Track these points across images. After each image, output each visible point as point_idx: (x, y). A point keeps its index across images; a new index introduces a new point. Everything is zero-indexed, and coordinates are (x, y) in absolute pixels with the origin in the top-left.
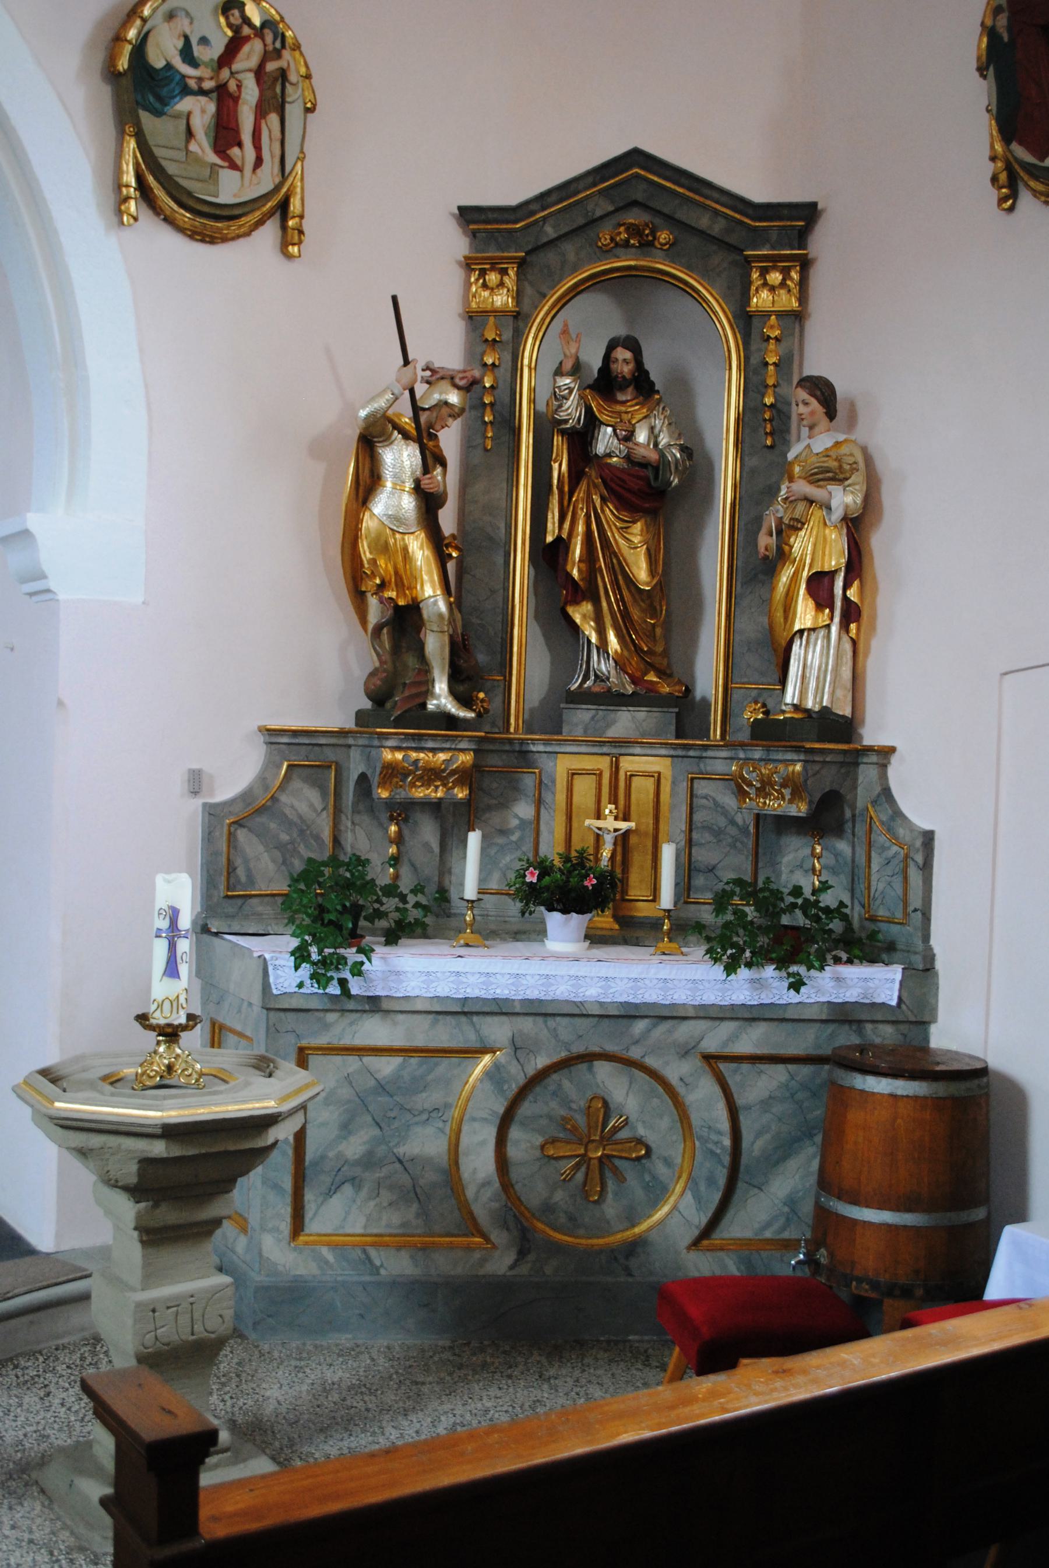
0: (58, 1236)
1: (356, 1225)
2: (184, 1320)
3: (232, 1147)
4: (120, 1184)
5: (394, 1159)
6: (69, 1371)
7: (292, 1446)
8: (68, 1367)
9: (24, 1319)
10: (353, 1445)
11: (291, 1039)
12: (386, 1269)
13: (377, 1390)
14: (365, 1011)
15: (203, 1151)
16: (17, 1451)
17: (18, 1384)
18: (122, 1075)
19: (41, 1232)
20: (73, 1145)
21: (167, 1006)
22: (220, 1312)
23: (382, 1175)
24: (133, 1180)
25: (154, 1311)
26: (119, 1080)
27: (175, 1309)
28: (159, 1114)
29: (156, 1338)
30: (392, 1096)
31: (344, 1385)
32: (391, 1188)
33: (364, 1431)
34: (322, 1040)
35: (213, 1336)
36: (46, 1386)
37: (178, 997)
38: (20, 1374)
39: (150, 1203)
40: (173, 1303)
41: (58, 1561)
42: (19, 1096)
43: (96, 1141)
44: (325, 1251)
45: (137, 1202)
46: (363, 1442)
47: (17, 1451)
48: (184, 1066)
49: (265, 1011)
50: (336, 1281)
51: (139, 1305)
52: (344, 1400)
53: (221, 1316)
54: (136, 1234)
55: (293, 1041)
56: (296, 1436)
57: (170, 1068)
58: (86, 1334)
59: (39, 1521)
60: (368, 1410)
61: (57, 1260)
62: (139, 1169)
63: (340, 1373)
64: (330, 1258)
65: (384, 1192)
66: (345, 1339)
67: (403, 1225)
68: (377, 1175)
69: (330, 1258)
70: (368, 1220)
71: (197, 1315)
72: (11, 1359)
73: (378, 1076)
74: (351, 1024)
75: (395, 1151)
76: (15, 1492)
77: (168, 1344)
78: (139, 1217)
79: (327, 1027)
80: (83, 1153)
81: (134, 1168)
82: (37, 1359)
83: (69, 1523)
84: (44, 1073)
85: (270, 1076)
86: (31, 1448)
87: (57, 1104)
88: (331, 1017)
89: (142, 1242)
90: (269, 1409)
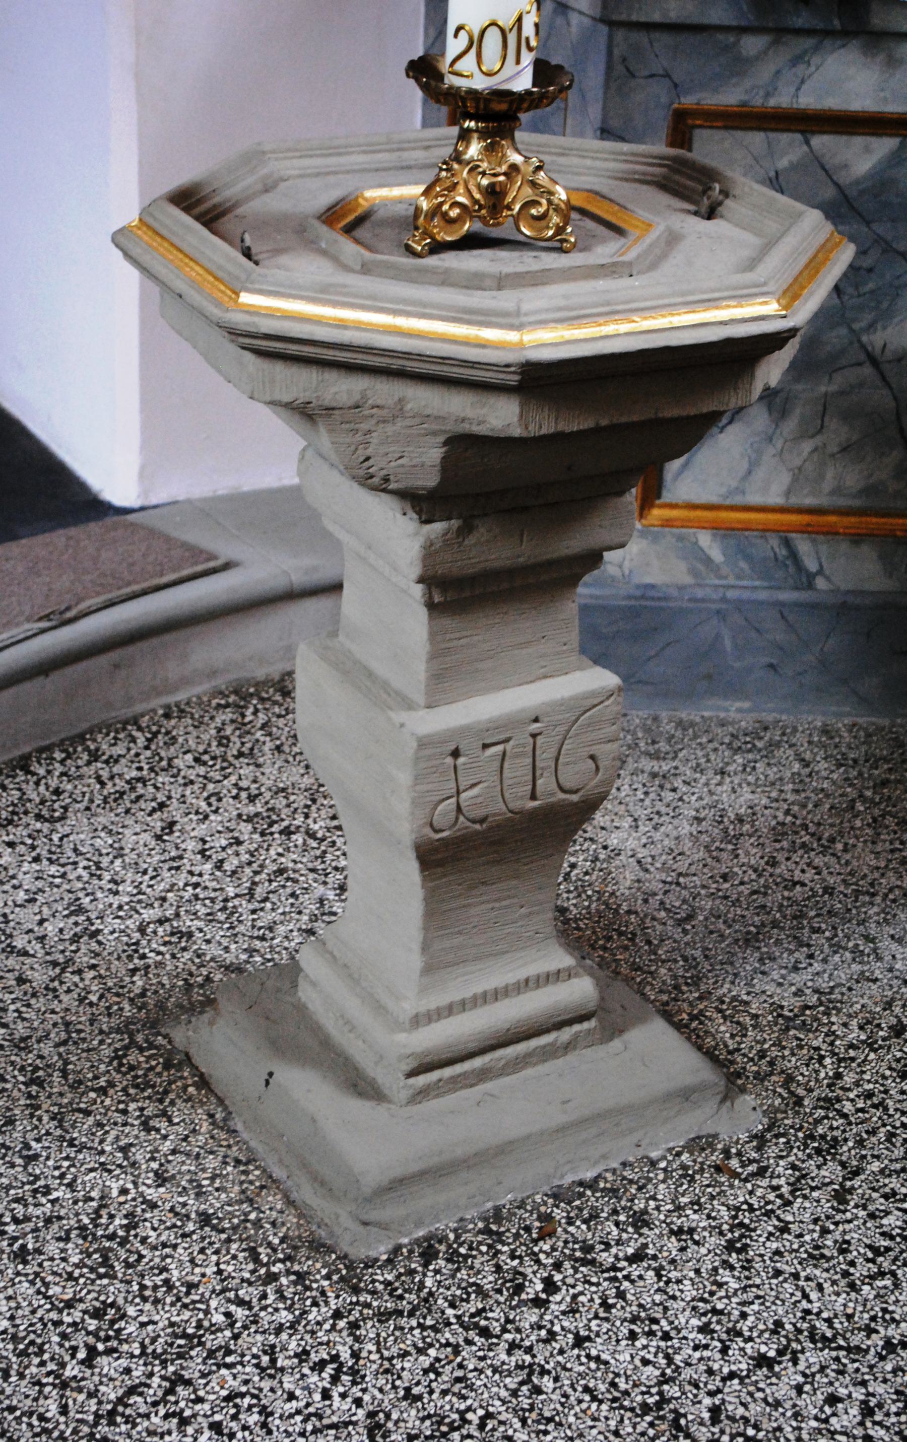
0: (144, 474)
1: (771, 487)
2: (517, 770)
3: (672, 412)
4: (392, 486)
5: (863, 357)
6: (202, 770)
7: (696, 981)
8: (196, 760)
9: (104, 661)
10: (823, 983)
11: (659, 91)
12: (828, 578)
13: (832, 840)
14: (828, 33)
15: (604, 422)
16: (134, 971)
17: (105, 801)
18: (364, 205)
19: (107, 457)
20: (287, 398)
21: (493, 40)
22: (594, 750)
23: (833, 388)
24: (430, 480)
25: (456, 754)
26: (361, 220)
27: (500, 748)
28: (512, 336)
29: (459, 809)
30: (868, 223)
31: (764, 823)
32: (846, 417)
33: (837, 948)
34: (729, 97)
35: (575, 798)
36: (162, 806)
37: (520, 20)
38: (105, 774)
39: (455, 523)
40: (494, 736)
41: (272, 1278)
42: (127, 255)
43: (342, 388)
44: (705, 539)
45: (428, 521)
46: (842, 976)
47: (134, 971)
48: (528, 193)
49: (604, 29)
50: (724, 599)
51: (424, 743)
52: (773, 862)
53: (592, 757)
54: (418, 590)
55: (664, 100)
56: (698, 953)
57: (495, 196)
58: (220, 682)
59: (211, 1162)
60: (829, 890)
61: (152, 533)
62: (445, 460)
63: (746, 795)
64: (716, 554)
65: (833, 423)
66: (738, 712)
67: (868, 491)
68: (823, 389)
69: (716, 554)
70: (795, 480)
71: (545, 758)
72: (81, 738)
73: (844, 179)
74: (796, 60)
75: (864, 339)
76: (148, 1085)
77: (482, 821)
78: (429, 553)
79: (740, 66)
80: (305, 413)
81: (434, 454)
82: (134, 740)
83: (278, 1173)
84: (186, 199)
85: (710, 215)
86: (159, 965)
87: (246, 298)
88: (752, 44)
89: (431, 606)
90: (626, 878)
